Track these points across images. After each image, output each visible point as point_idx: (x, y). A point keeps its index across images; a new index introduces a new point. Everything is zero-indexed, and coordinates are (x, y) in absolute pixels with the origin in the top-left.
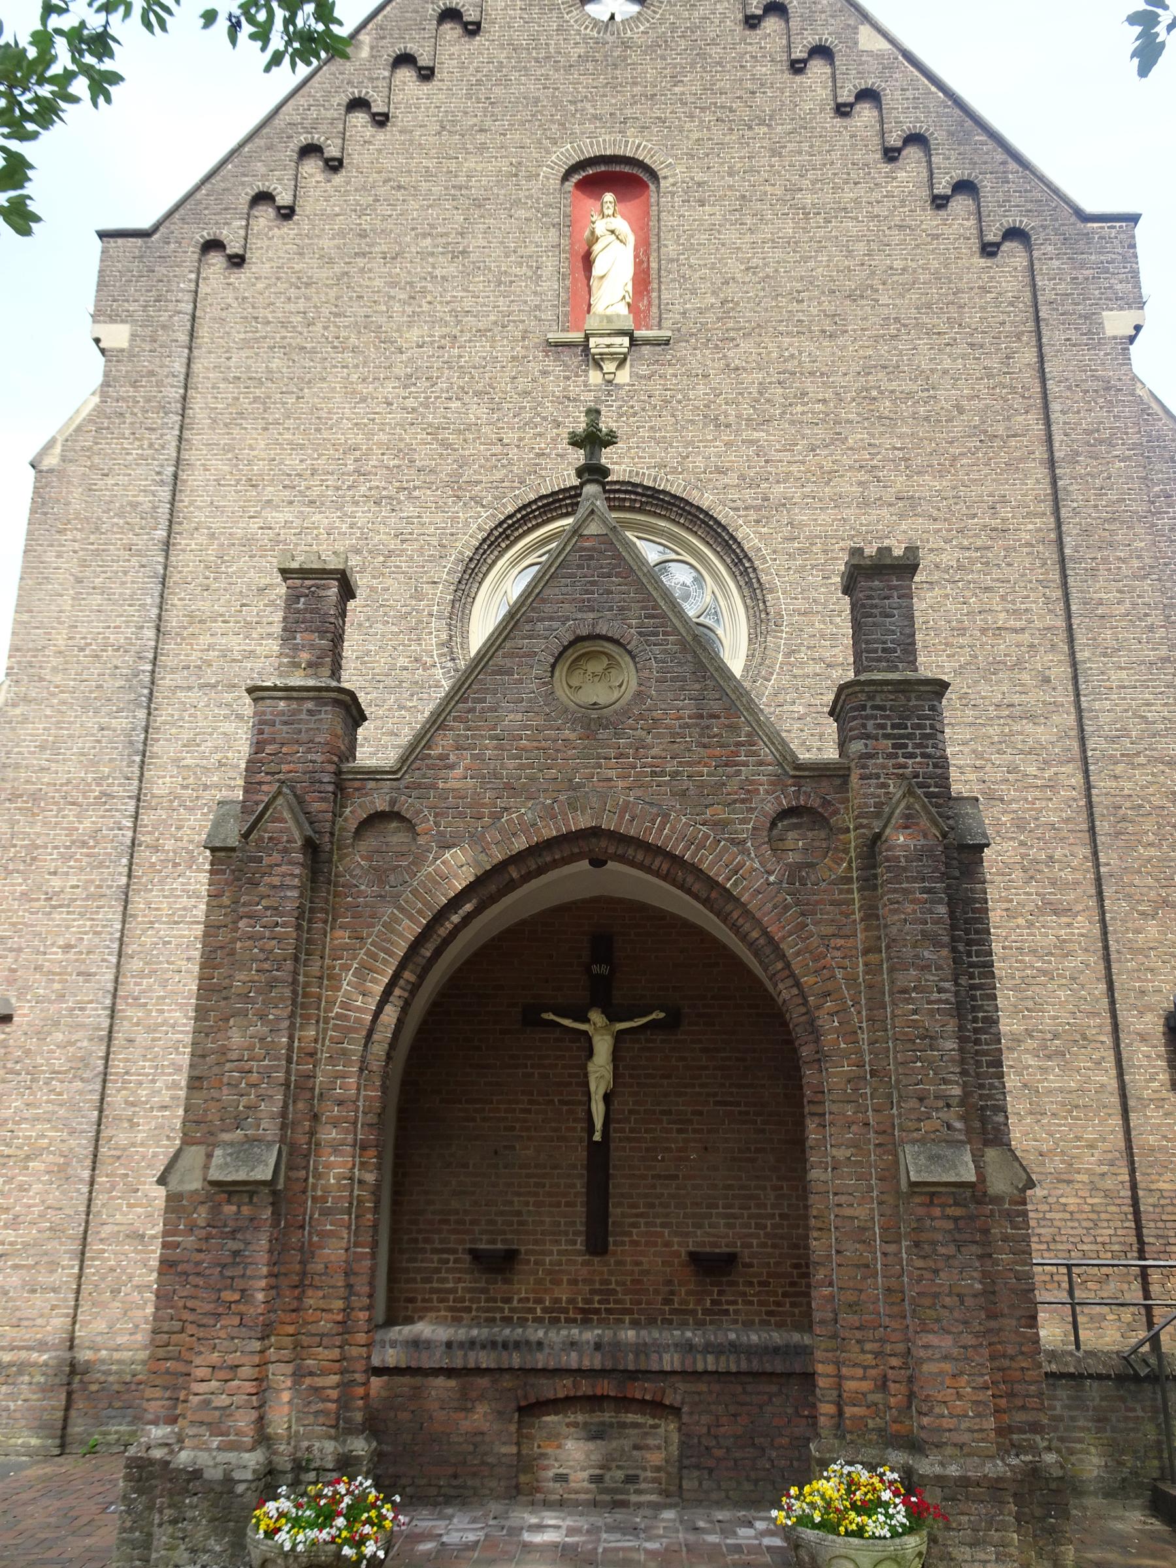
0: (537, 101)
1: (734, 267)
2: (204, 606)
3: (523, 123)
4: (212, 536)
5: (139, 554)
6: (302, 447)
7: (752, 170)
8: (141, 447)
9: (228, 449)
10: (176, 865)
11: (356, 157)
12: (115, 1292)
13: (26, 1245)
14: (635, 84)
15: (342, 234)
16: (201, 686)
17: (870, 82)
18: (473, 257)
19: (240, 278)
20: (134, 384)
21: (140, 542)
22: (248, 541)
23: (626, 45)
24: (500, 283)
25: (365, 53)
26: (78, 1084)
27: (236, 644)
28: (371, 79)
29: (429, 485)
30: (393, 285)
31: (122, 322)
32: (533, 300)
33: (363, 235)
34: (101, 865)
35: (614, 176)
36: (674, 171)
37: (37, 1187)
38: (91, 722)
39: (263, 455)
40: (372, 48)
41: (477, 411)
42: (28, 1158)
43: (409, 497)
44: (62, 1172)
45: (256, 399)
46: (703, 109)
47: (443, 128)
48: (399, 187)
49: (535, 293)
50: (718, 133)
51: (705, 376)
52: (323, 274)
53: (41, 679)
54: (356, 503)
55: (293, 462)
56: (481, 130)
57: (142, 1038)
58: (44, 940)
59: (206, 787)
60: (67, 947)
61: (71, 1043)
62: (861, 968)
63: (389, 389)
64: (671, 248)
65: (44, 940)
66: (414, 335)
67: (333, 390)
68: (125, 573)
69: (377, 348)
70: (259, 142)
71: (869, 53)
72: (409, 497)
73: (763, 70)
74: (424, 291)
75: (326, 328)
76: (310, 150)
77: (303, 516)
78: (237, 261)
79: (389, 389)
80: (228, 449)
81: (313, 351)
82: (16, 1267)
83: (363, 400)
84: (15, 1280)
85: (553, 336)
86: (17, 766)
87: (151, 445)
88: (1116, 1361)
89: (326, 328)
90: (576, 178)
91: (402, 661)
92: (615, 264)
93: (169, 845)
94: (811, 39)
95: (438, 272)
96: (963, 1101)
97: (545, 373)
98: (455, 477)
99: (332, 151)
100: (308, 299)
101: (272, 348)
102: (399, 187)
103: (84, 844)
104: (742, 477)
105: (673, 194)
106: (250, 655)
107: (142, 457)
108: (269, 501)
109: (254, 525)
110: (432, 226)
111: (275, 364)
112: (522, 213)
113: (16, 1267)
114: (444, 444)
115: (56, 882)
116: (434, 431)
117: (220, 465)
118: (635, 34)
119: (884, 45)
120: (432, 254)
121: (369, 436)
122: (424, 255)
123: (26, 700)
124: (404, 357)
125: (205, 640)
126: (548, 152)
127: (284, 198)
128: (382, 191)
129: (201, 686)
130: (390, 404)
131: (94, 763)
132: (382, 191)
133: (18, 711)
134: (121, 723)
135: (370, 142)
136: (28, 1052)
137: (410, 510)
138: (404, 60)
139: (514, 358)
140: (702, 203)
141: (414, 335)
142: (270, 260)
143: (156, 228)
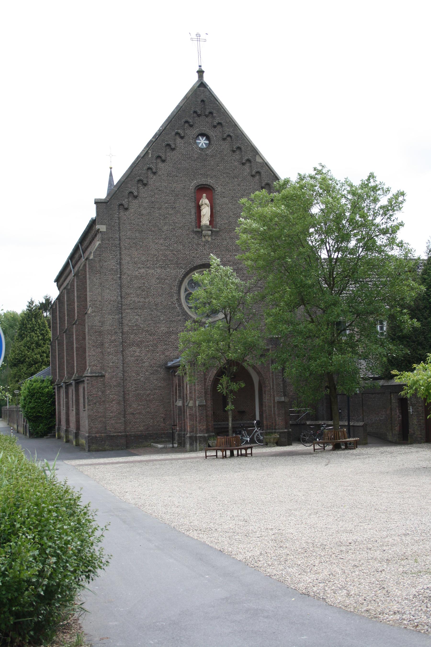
0: (188, 169)
1: (231, 214)
2: (128, 291)
3: (185, 175)
4: (128, 275)
5: (115, 280)
6: (144, 255)
7: (234, 190)
8: (112, 255)
9: (129, 255)
10: (130, 346)
11: (151, 182)
12: (130, 423)
13: (114, 416)
14: (209, 166)
15: (148, 202)
16: (130, 309)
17: (259, 170)
18: (177, 209)
19: (127, 213)
20: (109, 240)
21: (115, 277)
22: (136, 277)
23: (207, 155)
24: (183, 216)
25: (150, 156)
26: (119, 388)
27: (137, 300)
28: (152, 163)
29: (171, 264)
30: (160, 215)
31: (104, 225)
32: (190, 220)
33: (153, 202)
34: (117, 346)
35: (203, 189)
36: (219, 189)
37: (115, 406)
38: (110, 317)
39: (137, 256)
40: (151, 154)
41: (180, 247)
42: (112, 401)
43: (168, 267)
44: (119, 403)
45: (134, 243)
46: (224, 173)
47: (168, 175)
48: (160, 191)
49: (190, 218)
50: (227, 179)
51: (226, 240)
52: (144, 212)
53: (97, 307)
54: (157, 268)
55: (143, 258)
56: (177, 176)
57: (128, 379)
58: (108, 361)
59: (134, 330)
60: (113, 363)
61: (117, 380)
62: (351, 439)
63: (161, 241)
64: (218, 208)
65: (108, 361)
66: (166, 228)
67: (150, 241)
68: (113, 285)
69: (158, 231)
70: (129, 179)
71: (258, 162)
72: (168, 267)
73: (236, 164)
74: (167, 217)
75: (147, 226)
76: (140, 181)
77: (147, 271)
78: (126, 209)
79: (161, 241)
80: (129, 255)
81: (145, 231)
82: (113, 420)
83: (156, 244)
84: (113, 422)
85: (195, 229)
86: (95, 326)
87: (114, 255)
88: (23, 315)
89: (147, 226)
90: (197, 188)
91: (169, 303)
92: (206, 211)
93: (128, 342)
94: (246, 158)
95: (170, 212)
96: (283, 392)
97: (194, 238)
98: (177, 262)
99: (145, 182)
100: (142, 218)
101: (136, 231)
102: (160, 191)
103: (113, 342)
104: (233, 263)
105: (218, 195)
106: (139, 302)
107: (113, 258)
108: (139, 267)
109: (137, 273)
110: (168, 201)
111: (137, 235)
112: (186, 198)
113: (113, 420)
114: (174, 254)
115: (109, 350)
116: (172, 251)
117: (128, 259)
118: (209, 152)
119: (262, 161)
120: (168, 208)
121: (158, 252)
122: (167, 208)
123: (95, 312)
124: (164, 233)
125: (129, 299)
126: (191, 183)
127: (136, 194)
128: (156, 191)
129: (130, 309)
130: (162, 245)
131: (112, 326)
132: (156, 191)
133: (93, 314)
134: (117, 317)
135: (152, 178)
136: (109, 382)
137: (168, 270)
138: (159, 157)
139: (187, 234)
140: (224, 197)
141: (166, 228)
142: (133, 208)
143: (108, 201)
